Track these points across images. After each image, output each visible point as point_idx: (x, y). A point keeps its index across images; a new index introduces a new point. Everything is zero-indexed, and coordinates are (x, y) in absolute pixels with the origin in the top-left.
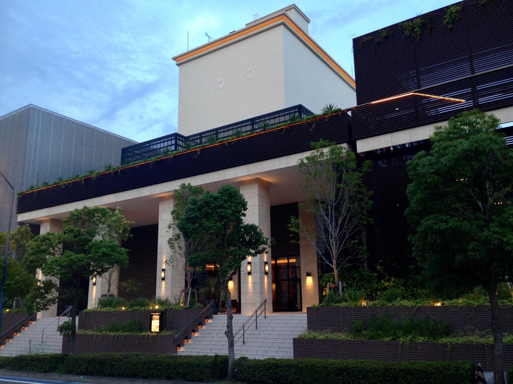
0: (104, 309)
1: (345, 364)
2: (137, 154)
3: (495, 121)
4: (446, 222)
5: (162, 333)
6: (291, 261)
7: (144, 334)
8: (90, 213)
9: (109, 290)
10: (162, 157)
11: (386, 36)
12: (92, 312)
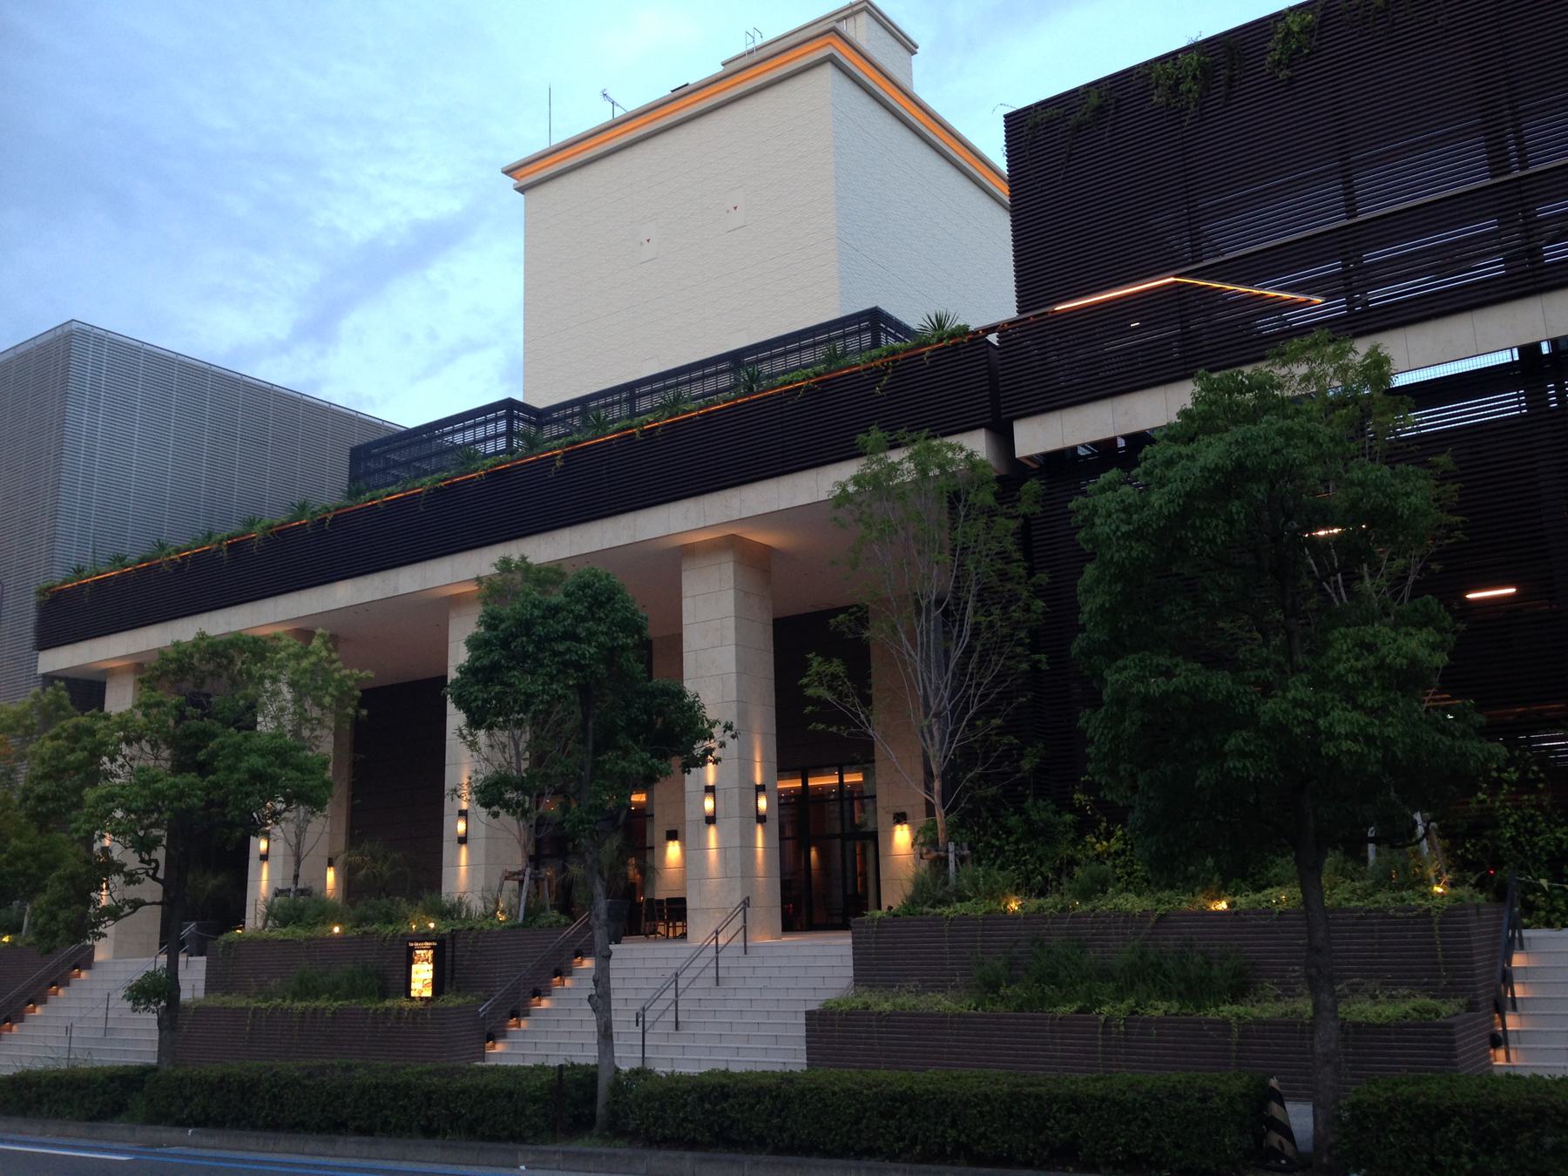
0: (280, 934)
1: (907, 1084)
2: (397, 465)
3: (1378, 367)
4: (1168, 674)
5: (439, 1003)
6: (848, 779)
7: (388, 1003)
8: (220, 651)
9: (296, 877)
10: (451, 475)
11: (1100, 107)
12: (259, 944)
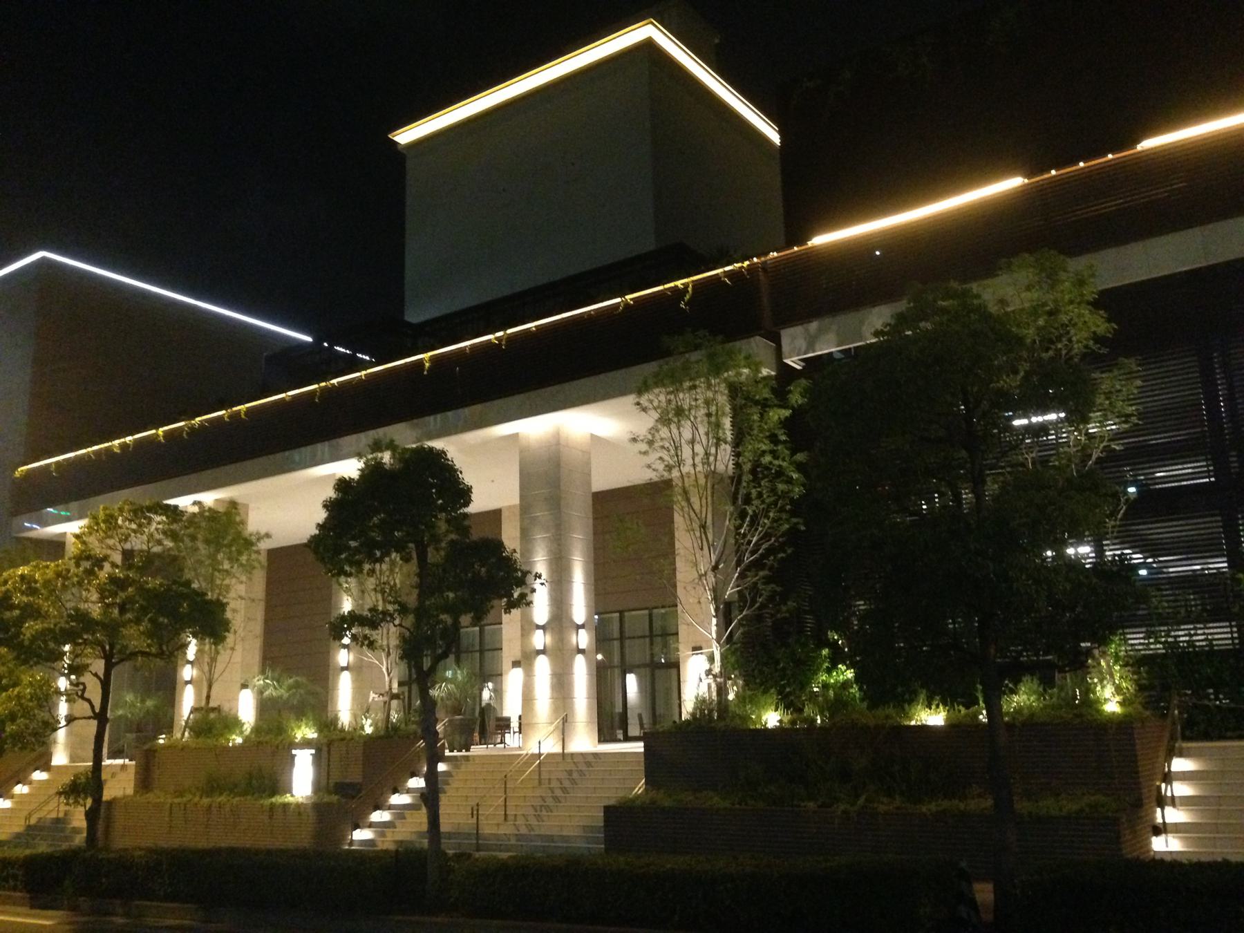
9: (208, 697)
